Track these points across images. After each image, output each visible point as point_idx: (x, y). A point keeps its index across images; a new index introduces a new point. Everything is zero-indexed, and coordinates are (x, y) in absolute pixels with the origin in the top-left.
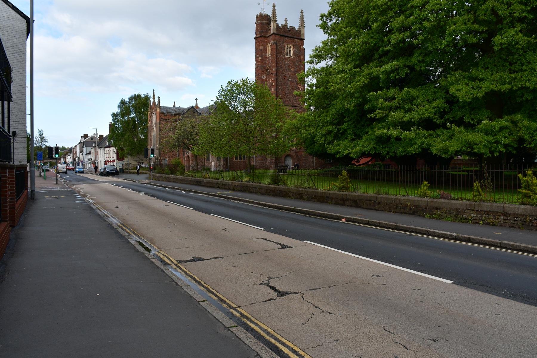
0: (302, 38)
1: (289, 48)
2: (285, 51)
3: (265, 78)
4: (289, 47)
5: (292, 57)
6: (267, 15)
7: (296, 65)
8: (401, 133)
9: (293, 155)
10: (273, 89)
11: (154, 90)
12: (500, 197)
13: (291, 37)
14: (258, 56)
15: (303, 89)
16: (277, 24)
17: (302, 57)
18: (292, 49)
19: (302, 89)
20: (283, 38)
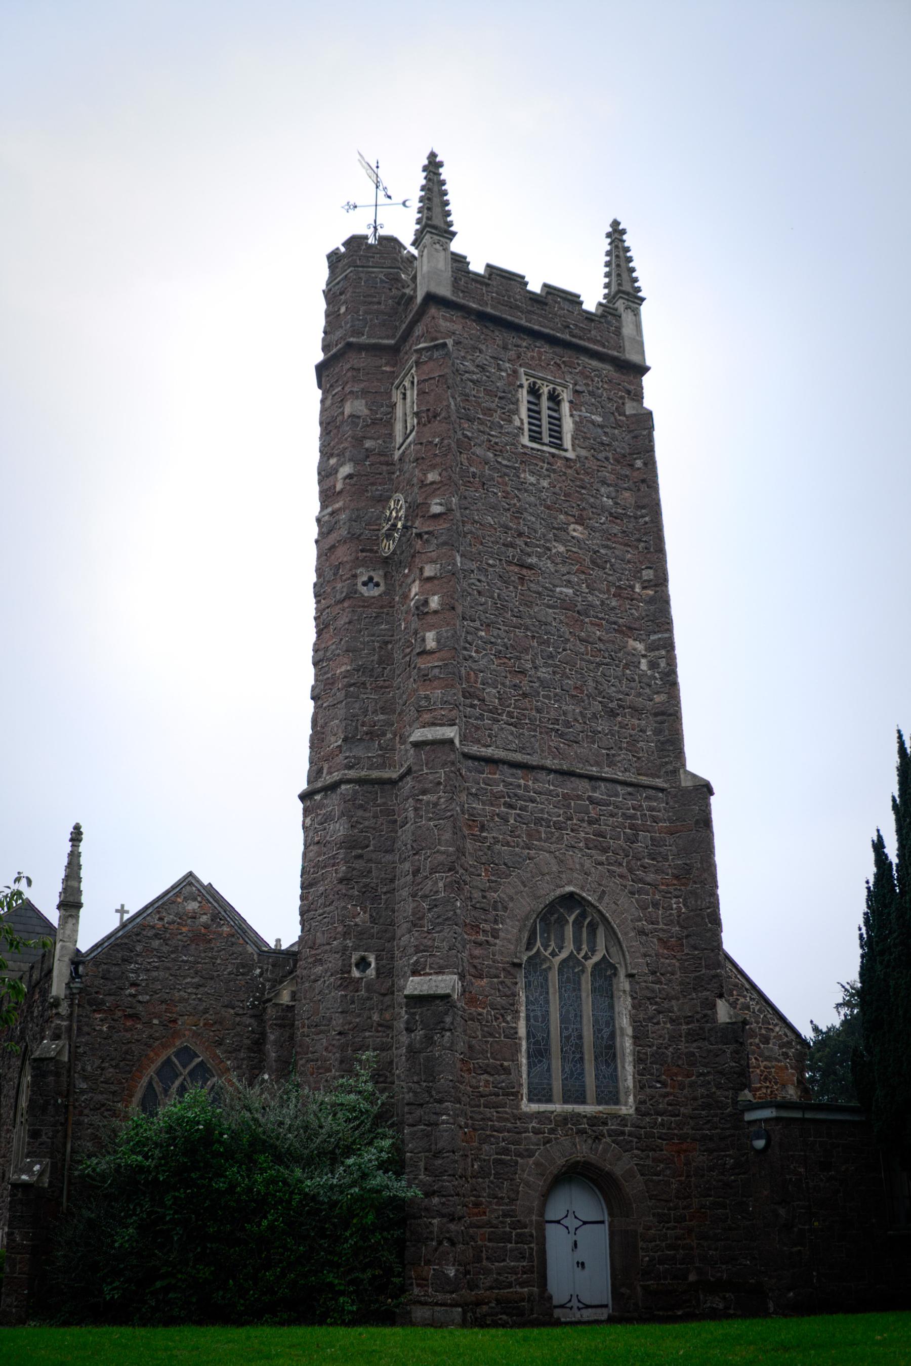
0: (633, 357)
1: (545, 403)
2: (516, 412)
3: (376, 592)
4: (545, 390)
5: (571, 455)
6: (390, 243)
7: (603, 509)
8: (628, 1035)
9: (618, 1170)
10: (430, 636)
11: (76, 836)
12: (730, 1093)
13: (552, 341)
14: (333, 461)
15: (663, 663)
16: (459, 261)
17: (639, 463)
18: (565, 407)
19: (653, 665)
20: (499, 336)
